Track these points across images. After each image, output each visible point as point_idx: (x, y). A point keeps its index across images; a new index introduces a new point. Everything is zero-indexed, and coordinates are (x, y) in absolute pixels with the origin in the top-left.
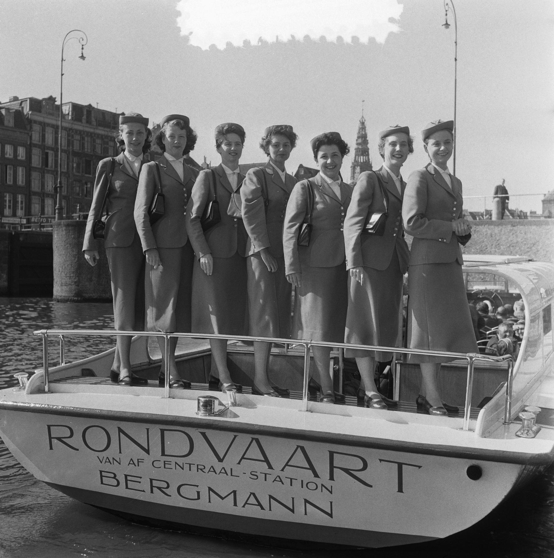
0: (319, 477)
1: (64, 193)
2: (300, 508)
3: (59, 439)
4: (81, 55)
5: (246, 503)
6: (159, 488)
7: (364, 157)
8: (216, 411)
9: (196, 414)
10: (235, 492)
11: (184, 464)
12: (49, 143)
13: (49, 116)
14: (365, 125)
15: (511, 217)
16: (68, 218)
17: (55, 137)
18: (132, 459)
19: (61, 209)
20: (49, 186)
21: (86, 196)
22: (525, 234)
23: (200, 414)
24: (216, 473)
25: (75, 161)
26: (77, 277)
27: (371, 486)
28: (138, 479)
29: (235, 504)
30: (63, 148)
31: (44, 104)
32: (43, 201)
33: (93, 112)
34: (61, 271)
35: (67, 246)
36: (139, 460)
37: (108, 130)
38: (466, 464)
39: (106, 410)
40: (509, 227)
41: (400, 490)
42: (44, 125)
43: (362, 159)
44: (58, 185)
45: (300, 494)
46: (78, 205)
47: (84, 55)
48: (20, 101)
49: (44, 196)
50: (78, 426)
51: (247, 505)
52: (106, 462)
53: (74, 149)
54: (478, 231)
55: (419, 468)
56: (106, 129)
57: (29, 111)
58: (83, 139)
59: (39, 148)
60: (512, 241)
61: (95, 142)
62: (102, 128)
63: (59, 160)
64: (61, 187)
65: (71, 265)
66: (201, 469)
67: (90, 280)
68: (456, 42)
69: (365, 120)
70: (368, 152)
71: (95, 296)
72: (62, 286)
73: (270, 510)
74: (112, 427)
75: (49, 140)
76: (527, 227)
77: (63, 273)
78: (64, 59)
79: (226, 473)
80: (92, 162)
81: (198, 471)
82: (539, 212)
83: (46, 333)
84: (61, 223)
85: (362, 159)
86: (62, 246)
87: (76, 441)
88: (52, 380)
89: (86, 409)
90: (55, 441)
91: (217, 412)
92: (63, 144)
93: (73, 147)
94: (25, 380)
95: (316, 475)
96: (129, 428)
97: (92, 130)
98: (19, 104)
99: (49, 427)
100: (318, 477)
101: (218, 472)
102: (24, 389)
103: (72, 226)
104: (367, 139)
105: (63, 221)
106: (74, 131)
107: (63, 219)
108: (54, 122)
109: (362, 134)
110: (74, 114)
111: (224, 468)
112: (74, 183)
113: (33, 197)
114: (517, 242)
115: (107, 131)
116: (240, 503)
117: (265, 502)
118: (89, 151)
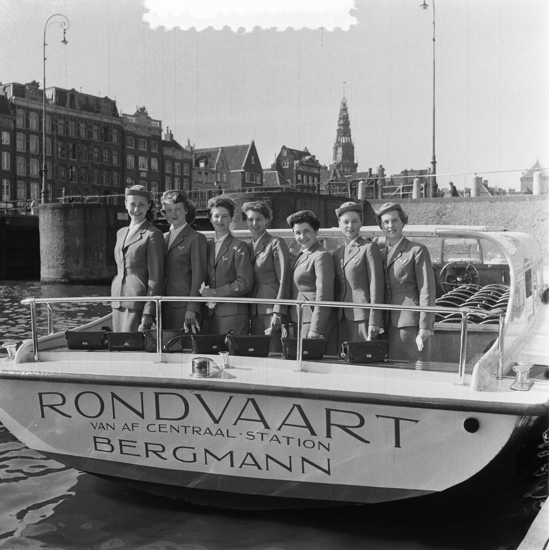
0: (270, 429)
1: (49, 178)
2: (297, 464)
3: (52, 407)
4: (63, 39)
5: (243, 463)
6: (155, 452)
7: (346, 138)
8: (211, 373)
9: (190, 376)
10: (231, 453)
11: (180, 427)
12: (34, 174)
13: (33, 101)
14: (347, 106)
15: (489, 194)
16: (54, 201)
17: (39, 121)
18: (126, 424)
19: (46, 192)
20: (35, 171)
21: (72, 180)
22: (503, 210)
23: (195, 376)
24: (212, 435)
25: (59, 145)
26: (64, 259)
27: (368, 442)
28: (133, 444)
29: (232, 465)
30: (47, 132)
31: (27, 89)
32: (28, 186)
33: (76, 96)
34: (48, 253)
35: (53, 229)
36: (134, 425)
37: (92, 114)
38: (463, 417)
39: (99, 375)
40: (488, 203)
41: (398, 445)
42: (28, 110)
43: (343, 140)
44: (43, 169)
45: (298, 453)
46: (64, 189)
47: (67, 40)
48: (3, 87)
49: (29, 181)
50: (71, 392)
51: (243, 465)
52: (99, 428)
53: (59, 133)
54: (457, 208)
55: (416, 422)
56: (89, 113)
57: (13, 96)
58: (67, 123)
59: (23, 133)
60: (490, 216)
61: (79, 126)
62: (85, 112)
63: (44, 144)
64: (46, 171)
65: (58, 248)
66: (196, 431)
67: (77, 262)
68: (434, 23)
69: (346, 102)
70: (350, 133)
71: (82, 277)
72: (49, 268)
73: (267, 469)
74: (106, 393)
75: (33, 125)
76: (504, 203)
77: (50, 256)
78: (46, 43)
79: (222, 434)
80: (76, 146)
81: (193, 433)
82: (518, 189)
83: (34, 301)
84: (47, 206)
85: (343, 140)
86: (48, 229)
87: (69, 408)
88: (42, 349)
89: (79, 375)
90: (46, 409)
91: (213, 373)
92: (47, 129)
93: (57, 131)
94: (14, 350)
95: (313, 433)
96: (121, 392)
97: (76, 115)
98: (2, 90)
99: (40, 395)
100: (315, 435)
101: (214, 433)
102: (13, 358)
103: (58, 208)
104: (349, 120)
105: (49, 205)
106: (58, 115)
107: (50, 203)
108: (37, 107)
109: (344, 115)
110: (58, 98)
111: (219, 429)
112: (59, 167)
113: (19, 182)
114: (495, 218)
115: (91, 115)
116: (237, 464)
117: (262, 462)
118: (74, 135)
